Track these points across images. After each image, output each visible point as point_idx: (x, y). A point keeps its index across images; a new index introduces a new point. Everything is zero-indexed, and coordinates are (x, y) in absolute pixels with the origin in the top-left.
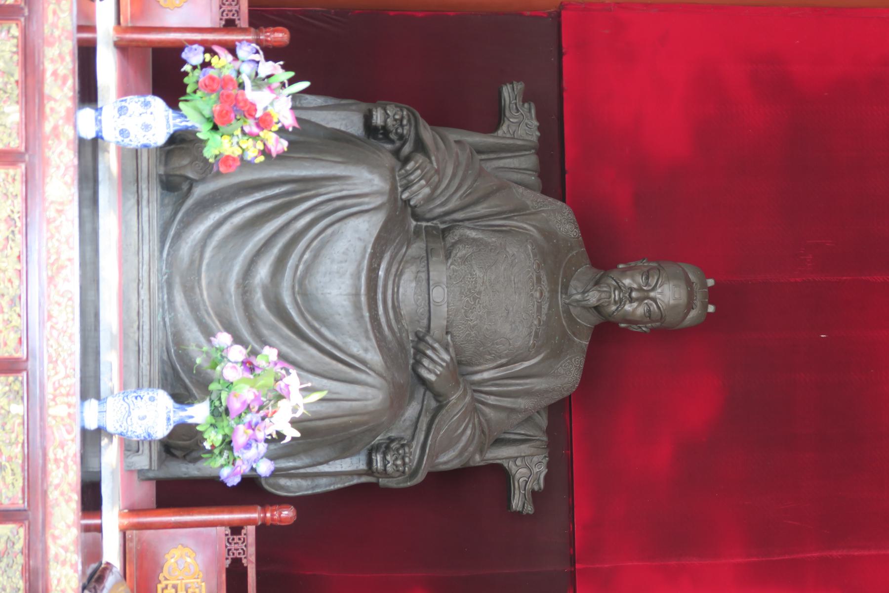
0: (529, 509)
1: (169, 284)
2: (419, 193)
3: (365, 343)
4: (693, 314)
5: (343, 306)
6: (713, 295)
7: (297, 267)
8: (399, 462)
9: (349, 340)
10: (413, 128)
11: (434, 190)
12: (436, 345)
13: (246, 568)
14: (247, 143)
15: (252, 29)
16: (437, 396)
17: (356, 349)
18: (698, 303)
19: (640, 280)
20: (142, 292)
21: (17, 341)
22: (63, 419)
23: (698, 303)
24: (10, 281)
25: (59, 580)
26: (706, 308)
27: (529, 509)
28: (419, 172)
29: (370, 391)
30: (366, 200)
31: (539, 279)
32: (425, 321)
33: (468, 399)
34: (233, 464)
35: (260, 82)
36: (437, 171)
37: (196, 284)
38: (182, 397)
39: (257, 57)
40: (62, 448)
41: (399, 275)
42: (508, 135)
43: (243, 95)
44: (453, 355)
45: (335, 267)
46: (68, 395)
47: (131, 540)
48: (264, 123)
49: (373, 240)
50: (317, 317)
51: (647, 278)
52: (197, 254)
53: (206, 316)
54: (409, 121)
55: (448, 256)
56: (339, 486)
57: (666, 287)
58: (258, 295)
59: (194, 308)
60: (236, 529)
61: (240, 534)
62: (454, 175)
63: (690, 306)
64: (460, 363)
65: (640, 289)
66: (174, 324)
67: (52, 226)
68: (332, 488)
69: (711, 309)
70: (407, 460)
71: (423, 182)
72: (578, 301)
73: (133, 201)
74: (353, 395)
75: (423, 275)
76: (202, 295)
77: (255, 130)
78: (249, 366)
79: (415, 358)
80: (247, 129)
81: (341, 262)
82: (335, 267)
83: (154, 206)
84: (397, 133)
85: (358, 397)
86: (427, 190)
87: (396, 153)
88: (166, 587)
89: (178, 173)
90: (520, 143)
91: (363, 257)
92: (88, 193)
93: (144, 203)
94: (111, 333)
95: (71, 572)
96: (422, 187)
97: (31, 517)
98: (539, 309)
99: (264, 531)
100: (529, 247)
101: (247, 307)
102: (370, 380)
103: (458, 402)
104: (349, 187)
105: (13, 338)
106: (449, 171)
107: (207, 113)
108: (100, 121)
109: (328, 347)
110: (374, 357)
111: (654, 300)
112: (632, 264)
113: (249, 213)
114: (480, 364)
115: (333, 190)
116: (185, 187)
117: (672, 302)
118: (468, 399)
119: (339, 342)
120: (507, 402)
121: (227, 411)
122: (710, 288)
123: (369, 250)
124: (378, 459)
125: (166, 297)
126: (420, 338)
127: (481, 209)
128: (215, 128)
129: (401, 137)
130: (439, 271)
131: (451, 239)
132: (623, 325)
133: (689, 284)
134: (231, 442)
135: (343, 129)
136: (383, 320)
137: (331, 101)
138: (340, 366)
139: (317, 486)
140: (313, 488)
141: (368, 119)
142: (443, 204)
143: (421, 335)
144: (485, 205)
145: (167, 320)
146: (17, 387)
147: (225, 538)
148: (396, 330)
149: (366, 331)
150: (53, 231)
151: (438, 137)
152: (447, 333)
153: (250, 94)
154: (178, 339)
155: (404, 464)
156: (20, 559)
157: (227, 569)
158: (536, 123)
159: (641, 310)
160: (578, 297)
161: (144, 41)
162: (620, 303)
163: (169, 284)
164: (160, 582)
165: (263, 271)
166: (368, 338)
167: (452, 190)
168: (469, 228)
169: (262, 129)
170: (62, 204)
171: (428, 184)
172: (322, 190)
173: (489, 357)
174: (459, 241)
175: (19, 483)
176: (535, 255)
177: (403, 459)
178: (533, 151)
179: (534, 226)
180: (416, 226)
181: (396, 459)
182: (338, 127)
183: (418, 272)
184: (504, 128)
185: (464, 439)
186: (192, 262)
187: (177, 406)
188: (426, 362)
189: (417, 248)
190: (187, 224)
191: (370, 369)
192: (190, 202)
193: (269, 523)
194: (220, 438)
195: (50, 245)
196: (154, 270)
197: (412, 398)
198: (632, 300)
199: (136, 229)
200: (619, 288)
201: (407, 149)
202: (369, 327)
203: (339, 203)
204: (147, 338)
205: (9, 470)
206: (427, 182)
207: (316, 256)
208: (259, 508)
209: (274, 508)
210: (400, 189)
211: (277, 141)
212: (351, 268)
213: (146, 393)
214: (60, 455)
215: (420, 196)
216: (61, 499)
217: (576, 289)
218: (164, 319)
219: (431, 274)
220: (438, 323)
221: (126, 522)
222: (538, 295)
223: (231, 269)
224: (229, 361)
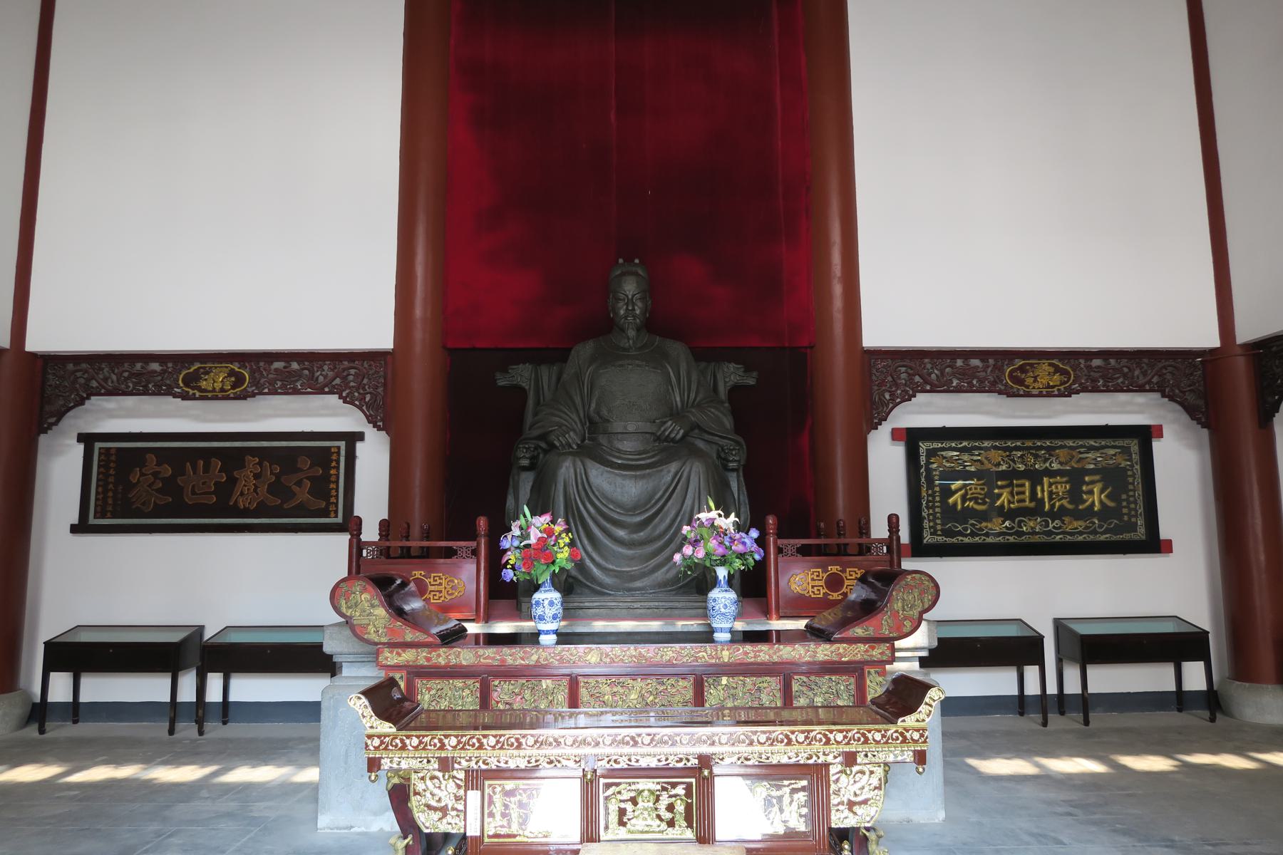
0: (755, 374)
1: (630, 590)
2: (573, 438)
3: (665, 472)
4: (640, 272)
5: (642, 485)
6: (629, 260)
7: (618, 513)
8: (734, 453)
9: (663, 482)
10: (531, 441)
11: (571, 430)
12: (662, 429)
13: (802, 545)
14: (561, 542)
15: (478, 539)
16: (692, 429)
17: (669, 478)
18: (634, 269)
19: (621, 304)
20: (636, 606)
21: (683, 681)
22: (730, 654)
23: (634, 269)
24: (647, 685)
25: (825, 655)
26: (636, 264)
27: (755, 374)
28: (560, 438)
29: (694, 469)
30: (578, 470)
31: (621, 366)
32: (647, 435)
33: (694, 410)
34: (753, 552)
35: (525, 536)
36: (560, 427)
37: (629, 574)
38: (714, 583)
39: (509, 537)
40: (748, 653)
41: (619, 451)
42: (528, 383)
43: (534, 545)
44: (668, 419)
45: (619, 490)
46: (717, 650)
47: (785, 613)
48: (550, 532)
49: (603, 467)
50: (646, 504)
51: (620, 300)
52: (611, 573)
53: (648, 568)
54: (526, 443)
55: (608, 421)
56: (744, 488)
57: (626, 288)
58: (635, 536)
59: (643, 575)
60: (779, 551)
61: (782, 548)
62: (561, 417)
63: (636, 274)
64: (671, 415)
65: (627, 304)
66: (653, 587)
67: (616, 660)
68: (745, 493)
69: (637, 261)
70: (732, 448)
71: (567, 436)
72: (634, 343)
73: (580, 612)
74: (697, 479)
75: (620, 436)
76: (636, 570)
77: (554, 538)
78: (695, 543)
79: (669, 442)
80: (552, 543)
81: (616, 486)
82: (619, 490)
83: (583, 599)
84: (534, 451)
85: (698, 476)
86: (572, 433)
87: (546, 452)
88: (813, 592)
89: (563, 584)
90: (533, 375)
91: (613, 473)
92: (576, 638)
93: (582, 605)
94: (663, 625)
95: (821, 648)
96: (570, 436)
97: (789, 672)
98: (638, 366)
99: (780, 534)
100: (601, 371)
101: (642, 543)
102: (687, 470)
103: (695, 416)
104: (571, 481)
105: (682, 683)
106: (557, 419)
107: (545, 567)
108: (547, 631)
109: (668, 494)
110: (673, 467)
111: (633, 296)
112: (610, 308)
113: (586, 542)
114: (672, 404)
115: (572, 490)
116: (571, 580)
117: (635, 285)
118: (694, 410)
119: (664, 487)
120: (694, 387)
121: (723, 556)
122: (624, 261)
123: (609, 469)
124: (731, 465)
125: (637, 592)
126: (658, 439)
127: (578, 400)
128: (553, 563)
129: (536, 448)
130: (617, 426)
131: (597, 419)
132: (648, 315)
133: (623, 274)
134: (741, 554)
135: (531, 484)
136: (648, 461)
137: (511, 490)
138: (679, 487)
139: (744, 502)
140: (745, 504)
141: (525, 469)
142: (575, 423)
143: (656, 438)
144: (575, 397)
145: (651, 591)
146: (711, 681)
147: (785, 558)
148: (653, 453)
149: (658, 471)
150: (618, 659)
151: (537, 425)
152: (654, 422)
153: (533, 540)
154: (663, 585)
155: (734, 449)
156: (813, 678)
157: (803, 556)
158: (521, 366)
159: (640, 304)
160: (631, 342)
161: (485, 604)
162: (635, 316)
163: (630, 590)
164: (810, 596)
165: (621, 533)
166: (661, 471)
167: (568, 418)
168: (589, 408)
169: (554, 534)
170: (602, 654)
171: (568, 433)
172: (572, 497)
173: (668, 397)
174: (598, 414)
175: (768, 679)
176: (606, 368)
177: (730, 450)
178: (538, 367)
179: (588, 368)
180: (589, 440)
181: (732, 454)
182: (530, 488)
183: (618, 439)
184: (524, 385)
185: (717, 413)
186: (616, 577)
187: (718, 586)
188: (673, 435)
189: (603, 440)
190: (593, 579)
191: (681, 469)
192: (580, 577)
193: (776, 531)
194: (737, 560)
195: (627, 661)
196: (622, 599)
197: (693, 444)
198: (634, 309)
199: (598, 610)
200: (626, 318)
201: (543, 445)
202: (654, 470)
203: (580, 487)
204: (663, 604)
205: (760, 685)
206: (567, 433)
207: (612, 502)
208: (767, 537)
209: (767, 528)
210: (571, 450)
211: (559, 525)
212: (619, 480)
213: (710, 604)
214: (752, 655)
215: (575, 437)
216: (778, 654)
217: (625, 343)
218: (651, 593)
219: (619, 431)
220: (648, 427)
221: (774, 616)
222: (630, 367)
223: (620, 553)
224: (693, 554)
